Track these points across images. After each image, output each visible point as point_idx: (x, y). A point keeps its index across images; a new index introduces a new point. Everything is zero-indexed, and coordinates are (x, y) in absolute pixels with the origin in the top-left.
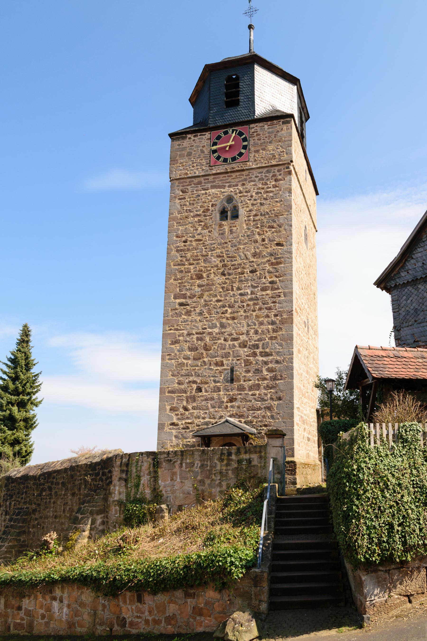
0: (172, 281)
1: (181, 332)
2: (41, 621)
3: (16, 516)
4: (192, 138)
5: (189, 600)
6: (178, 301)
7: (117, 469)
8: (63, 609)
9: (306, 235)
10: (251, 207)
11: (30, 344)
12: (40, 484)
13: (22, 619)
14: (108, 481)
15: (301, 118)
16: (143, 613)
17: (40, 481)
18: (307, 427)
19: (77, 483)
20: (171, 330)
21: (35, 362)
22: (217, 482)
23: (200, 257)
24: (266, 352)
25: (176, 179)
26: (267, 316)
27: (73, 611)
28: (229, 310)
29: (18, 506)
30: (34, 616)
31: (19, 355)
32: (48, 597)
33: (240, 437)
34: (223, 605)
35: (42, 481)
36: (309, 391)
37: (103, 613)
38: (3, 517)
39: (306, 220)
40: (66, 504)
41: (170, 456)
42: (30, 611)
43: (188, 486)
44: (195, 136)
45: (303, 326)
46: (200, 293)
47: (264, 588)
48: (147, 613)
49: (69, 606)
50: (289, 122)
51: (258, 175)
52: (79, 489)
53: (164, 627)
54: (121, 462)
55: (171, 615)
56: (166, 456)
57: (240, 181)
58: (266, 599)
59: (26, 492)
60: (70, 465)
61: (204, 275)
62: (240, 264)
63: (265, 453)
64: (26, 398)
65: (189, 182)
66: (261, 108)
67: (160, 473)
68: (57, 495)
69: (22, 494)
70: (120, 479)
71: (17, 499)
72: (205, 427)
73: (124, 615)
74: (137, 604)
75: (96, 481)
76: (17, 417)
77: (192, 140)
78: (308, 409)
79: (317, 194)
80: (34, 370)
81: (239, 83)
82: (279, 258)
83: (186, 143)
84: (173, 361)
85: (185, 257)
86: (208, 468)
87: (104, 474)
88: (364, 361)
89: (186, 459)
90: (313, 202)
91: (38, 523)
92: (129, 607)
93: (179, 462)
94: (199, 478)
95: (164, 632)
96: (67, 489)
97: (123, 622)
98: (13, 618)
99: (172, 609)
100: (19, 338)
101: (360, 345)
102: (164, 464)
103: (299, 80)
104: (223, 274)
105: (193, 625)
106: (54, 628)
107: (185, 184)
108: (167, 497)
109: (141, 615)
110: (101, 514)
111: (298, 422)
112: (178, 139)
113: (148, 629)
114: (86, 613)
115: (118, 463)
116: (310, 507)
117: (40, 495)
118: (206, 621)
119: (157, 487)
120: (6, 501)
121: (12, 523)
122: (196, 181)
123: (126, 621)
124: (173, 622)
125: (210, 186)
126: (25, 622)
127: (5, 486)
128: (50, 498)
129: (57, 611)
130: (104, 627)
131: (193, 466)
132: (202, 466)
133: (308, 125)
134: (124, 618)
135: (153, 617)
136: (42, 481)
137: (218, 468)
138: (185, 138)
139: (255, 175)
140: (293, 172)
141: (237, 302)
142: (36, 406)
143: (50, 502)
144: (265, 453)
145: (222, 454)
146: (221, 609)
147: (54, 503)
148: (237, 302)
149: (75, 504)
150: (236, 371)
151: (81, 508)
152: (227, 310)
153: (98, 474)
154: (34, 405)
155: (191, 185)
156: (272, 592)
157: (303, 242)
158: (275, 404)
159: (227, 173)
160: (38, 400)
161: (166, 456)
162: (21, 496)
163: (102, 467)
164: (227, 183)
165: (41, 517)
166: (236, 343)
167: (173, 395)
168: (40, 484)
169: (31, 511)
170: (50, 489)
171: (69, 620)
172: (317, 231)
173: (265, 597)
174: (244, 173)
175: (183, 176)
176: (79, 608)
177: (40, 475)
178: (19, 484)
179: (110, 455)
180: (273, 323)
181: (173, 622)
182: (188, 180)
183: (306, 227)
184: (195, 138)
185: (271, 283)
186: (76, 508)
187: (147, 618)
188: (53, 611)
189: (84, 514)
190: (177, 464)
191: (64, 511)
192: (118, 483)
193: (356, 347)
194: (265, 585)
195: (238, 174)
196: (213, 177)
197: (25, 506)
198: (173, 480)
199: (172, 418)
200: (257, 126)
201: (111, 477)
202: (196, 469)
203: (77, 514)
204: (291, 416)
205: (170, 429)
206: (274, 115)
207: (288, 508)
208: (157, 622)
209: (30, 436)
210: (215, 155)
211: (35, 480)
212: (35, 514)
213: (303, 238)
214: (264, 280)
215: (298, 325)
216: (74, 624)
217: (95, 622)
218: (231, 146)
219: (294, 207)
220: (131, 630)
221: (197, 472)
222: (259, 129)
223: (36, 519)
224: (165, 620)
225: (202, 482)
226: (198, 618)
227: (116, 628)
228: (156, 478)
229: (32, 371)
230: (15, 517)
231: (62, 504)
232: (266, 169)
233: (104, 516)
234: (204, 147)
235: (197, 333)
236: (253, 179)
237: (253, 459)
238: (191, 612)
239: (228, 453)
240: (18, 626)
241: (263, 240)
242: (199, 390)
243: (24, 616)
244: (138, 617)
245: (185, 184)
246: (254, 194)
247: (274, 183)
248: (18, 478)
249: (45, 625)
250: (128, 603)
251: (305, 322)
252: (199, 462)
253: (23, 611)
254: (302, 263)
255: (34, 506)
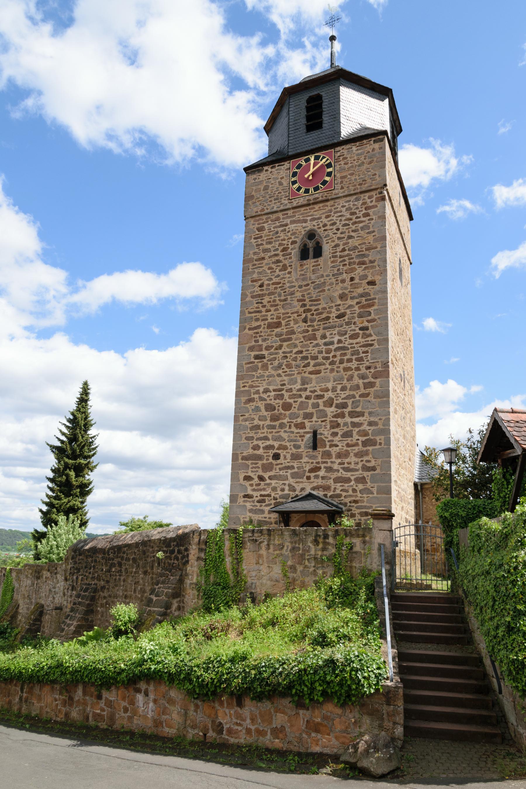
0: (247, 331)
1: (257, 389)
2: (123, 715)
3: (84, 592)
4: (270, 170)
5: (301, 712)
6: (253, 354)
7: (194, 547)
8: (148, 703)
9: (401, 271)
10: (337, 242)
11: (89, 402)
12: (110, 559)
13: (103, 710)
14: (184, 561)
15: (392, 132)
16: (244, 720)
17: (109, 555)
18: (404, 505)
19: (149, 560)
20: (244, 387)
21: (92, 422)
22: (312, 569)
23: (278, 302)
24: (356, 412)
25: (252, 217)
26: (358, 369)
27: (160, 707)
28: (312, 363)
29: (86, 581)
30: (115, 708)
31: (79, 416)
32: (131, 689)
33: (326, 515)
34: (346, 722)
35: (111, 555)
36: (406, 460)
37: (195, 714)
38: (70, 592)
39: (400, 251)
40: (137, 583)
41: (256, 535)
42: (111, 701)
43: (277, 571)
44: (272, 168)
45: (399, 379)
46: (278, 344)
47: (399, 707)
48: (248, 721)
49: (155, 701)
50: (382, 140)
51: (345, 204)
52: (152, 568)
53: (270, 740)
54: (200, 539)
55: (279, 727)
56: (250, 535)
57: (323, 214)
58: (402, 722)
59: (94, 566)
60: (142, 539)
61: (283, 323)
62: (324, 308)
63: (371, 538)
64: (82, 461)
65: (266, 219)
66: (347, 129)
67: (244, 555)
68: (127, 573)
69: (90, 569)
70: (199, 558)
71: (85, 573)
72: (284, 500)
73: (220, 719)
74: (236, 708)
75: (171, 560)
76: (74, 483)
77: (269, 172)
78: (406, 482)
79: (411, 218)
80: (92, 432)
81: (322, 103)
82: (370, 300)
83: (262, 176)
84: (247, 423)
85: (261, 303)
86: (301, 552)
87: (179, 552)
88: (508, 428)
89: (274, 540)
90: (407, 229)
91: (107, 602)
92: (227, 711)
93: (266, 543)
94: (289, 563)
95: (270, 746)
96: (138, 566)
97: (219, 728)
98: (92, 708)
99: (279, 720)
100: (79, 396)
101: (497, 408)
102: (249, 544)
103: (391, 90)
104: (305, 321)
105: (307, 743)
106: (138, 724)
107: (261, 222)
108: (252, 584)
109: (242, 722)
110: (177, 597)
111: (396, 499)
112: (254, 173)
113: (250, 740)
114: (176, 712)
115: (196, 540)
116: (425, 609)
117: (109, 571)
118: (324, 740)
119: (240, 570)
120: (73, 575)
121: (80, 600)
122: (273, 217)
123: (223, 727)
124: (281, 735)
125: (289, 222)
126: (105, 713)
127: (72, 558)
128: (120, 575)
129: (141, 705)
130: (196, 731)
131: (282, 548)
132: (293, 548)
133: (399, 138)
134: (221, 724)
135: (256, 726)
136: (111, 555)
137: (312, 552)
138: (260, 171)
139: (341, 205)
140: (387, 197)
141: (322, 352)
142: (92, 471)
143: (120, 579)
144: (371, 538)
145: (317, 536)
146: (343, 727)
147: (124, 581)
148: (322, 352)
149: (146, 584)
150: (321, 434)
151: (155, 589)
152: (309, 363)
153: (172, 552)
154: (90, 469)
155: (268, 222)
156: (408, 714)
157: (398, 279)
158: (368, 476)
159: (309, 205)
160: (94, 464)
161: (250, 535)
162: (89, 571)
163: (177, 543)
164: (309, 216)
165: (110, 596)
166: (320, 401)
167: (247, 462)
168: (110, 559)
169: (99, 588)
170: (120, 564)
171: (156, 717)
172: (411, 264)
173: (400, 719)
174: (328, 203)
175: (259, 213)
176: (167, 705)
177: (109, 549)
178: (87, 558)
179: (187, 531)
180: (363, 377)
181: (281, 735)
182: (264, 217)
183: (400, 261)
184: (273, 170)
185: (361, 329)
186: (148, 589)
187: (248, 726)
188: (137, 704)
189: (159, 596)
190: (264, 545)
191: (135, 591)
192: (196, 563)
193: (495, 410)
194: (400, 704)
195: (321, 205)
196: (292, 211)
197: (93, 582)
198: (258, 563)
199: (246, 488)
200: (343, 149)
201: (188, 555)
202: (286, 552)
203: (151, 596)
204: (388, 491)
205: (244, 501)
206: (363, 134)
207: (407, 608)
208: (261, 733)
209: (85, 504)
210: (294, 186)
211: (104, 554)
212: (103, 592)
213: (398, 274)
214: (353, 326)
215: (395, 379)
216: (161, 723)
217: (185, 723)
218: (313, 174)
219: (388, 237)
220: (229, 738)
221: (287, 556)
222: (345, 152)
223: (105, 598)
224: (271, 732)
225: (293, 568)
226: (313, 735)
227: (211, 734)
228: (238, 561)
229: (89, 432)
230: (83, 593)
231: (133, 583)
232: (355, 197)
233: (180, 601)
234: (282, 178)
235: (274, 390)
236: (339, 209)
237: (355, 544)
238: (304, 726)
239: (324, 535)
240: (98, 717)
241: (352, 279)
242: (276, 457)
243: (105, 707)
244: (237, 724)
245: (261, 222)
246: (340, 227)
247: (364, 211)
248: (86, 550)
249: (128, 719)
250: (225, 705)
251: (401, 375)
252: (289, 544)
253: (103, 701)
254: (397, 304)
255: (102, 583)
